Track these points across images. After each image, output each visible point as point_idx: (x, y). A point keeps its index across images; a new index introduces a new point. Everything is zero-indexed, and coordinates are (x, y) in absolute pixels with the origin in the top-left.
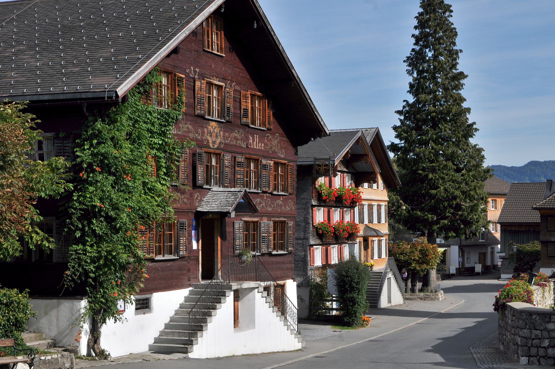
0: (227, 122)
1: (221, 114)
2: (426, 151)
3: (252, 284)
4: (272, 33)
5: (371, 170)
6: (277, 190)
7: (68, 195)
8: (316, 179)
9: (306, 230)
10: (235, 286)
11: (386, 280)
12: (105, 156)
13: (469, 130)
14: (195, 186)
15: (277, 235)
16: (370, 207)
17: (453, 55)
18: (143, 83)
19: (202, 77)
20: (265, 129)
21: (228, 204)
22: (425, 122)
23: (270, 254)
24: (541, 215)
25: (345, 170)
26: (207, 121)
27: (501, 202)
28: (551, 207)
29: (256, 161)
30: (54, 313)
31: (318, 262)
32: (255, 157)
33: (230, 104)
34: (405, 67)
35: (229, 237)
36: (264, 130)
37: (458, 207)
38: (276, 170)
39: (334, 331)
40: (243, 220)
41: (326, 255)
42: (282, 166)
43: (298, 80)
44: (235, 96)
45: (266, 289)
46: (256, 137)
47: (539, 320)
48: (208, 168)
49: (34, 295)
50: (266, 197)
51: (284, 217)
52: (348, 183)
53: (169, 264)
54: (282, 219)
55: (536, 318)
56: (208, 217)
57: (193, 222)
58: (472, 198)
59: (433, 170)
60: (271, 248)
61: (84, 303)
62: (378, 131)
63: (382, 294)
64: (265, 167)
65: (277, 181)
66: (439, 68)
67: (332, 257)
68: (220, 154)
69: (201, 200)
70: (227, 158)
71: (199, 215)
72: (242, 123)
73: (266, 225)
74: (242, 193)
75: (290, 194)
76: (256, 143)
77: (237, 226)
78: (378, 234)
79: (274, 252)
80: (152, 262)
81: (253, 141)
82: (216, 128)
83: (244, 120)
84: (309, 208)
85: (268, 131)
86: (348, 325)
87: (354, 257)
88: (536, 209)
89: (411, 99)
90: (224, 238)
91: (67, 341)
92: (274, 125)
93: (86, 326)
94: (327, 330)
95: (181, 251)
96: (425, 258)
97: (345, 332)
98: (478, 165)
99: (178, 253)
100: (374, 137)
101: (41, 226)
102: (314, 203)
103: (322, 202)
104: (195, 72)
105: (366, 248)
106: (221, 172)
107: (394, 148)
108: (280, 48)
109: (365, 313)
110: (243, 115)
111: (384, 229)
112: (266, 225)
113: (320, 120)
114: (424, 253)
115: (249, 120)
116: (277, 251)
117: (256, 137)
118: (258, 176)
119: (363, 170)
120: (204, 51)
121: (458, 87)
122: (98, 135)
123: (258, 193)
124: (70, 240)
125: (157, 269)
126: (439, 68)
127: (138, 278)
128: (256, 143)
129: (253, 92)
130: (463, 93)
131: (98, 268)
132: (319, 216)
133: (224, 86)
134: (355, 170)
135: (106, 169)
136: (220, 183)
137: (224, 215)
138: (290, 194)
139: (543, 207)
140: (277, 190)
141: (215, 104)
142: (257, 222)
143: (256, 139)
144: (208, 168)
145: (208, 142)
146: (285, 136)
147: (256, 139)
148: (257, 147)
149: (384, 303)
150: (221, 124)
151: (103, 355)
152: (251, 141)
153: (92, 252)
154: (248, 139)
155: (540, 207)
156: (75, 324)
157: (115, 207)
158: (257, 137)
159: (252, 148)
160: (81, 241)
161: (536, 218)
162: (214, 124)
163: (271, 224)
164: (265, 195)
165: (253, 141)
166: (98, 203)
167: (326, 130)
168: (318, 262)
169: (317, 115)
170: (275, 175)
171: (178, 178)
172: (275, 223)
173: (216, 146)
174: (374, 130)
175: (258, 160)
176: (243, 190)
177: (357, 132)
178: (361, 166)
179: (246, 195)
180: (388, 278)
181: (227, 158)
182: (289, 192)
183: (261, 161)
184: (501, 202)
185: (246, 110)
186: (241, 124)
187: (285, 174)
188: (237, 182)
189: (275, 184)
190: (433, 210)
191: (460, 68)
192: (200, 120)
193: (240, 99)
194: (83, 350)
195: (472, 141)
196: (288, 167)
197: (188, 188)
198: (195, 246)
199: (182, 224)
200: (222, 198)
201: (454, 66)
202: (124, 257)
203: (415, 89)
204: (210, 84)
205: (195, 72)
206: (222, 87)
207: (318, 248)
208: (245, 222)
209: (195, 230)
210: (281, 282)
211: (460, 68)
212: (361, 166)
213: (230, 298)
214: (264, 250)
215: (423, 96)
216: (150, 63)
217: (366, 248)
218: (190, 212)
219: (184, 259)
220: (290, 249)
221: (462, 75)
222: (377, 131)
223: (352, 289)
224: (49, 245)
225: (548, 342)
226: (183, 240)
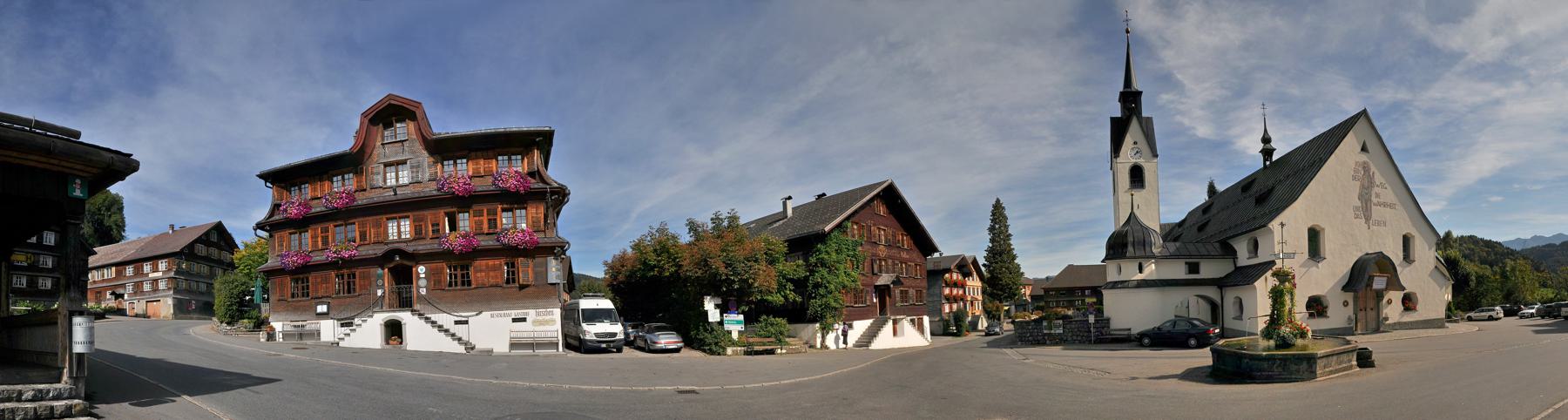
1: (886, 242)
2: (998, 266)
3: (902, 317)
7: (806, 278)
9: (941, 297)
10: (892, 317)
12: (822, 259)
13: (1014, 257)
14: (873, 274)
16: (973, 289)
17: (1007, 227)
18: (839, 226)
19: (874, 225)
22: (996, 254)
23: (914, 304)
27: (1031, 287)
29: (906, 263)
30: (806, 330)
31: (947, 310)
33: (890, 237)
34: (987, 232)
35: (893, 297)
37: (1011, 288)
41: (951, 308)
45: (912, 321)
48: (880, 266)
49: (790, 322)
52: (960, 277)
58: (1016, 284)
59: (1000, 274)
61: (818, 325)
66: (1001, 233)
67: (485, 189)
70: (890, 262)
73: (912, 292)
76: (904, 255)
78: (977, 300)
86: (959, 336)
87: (364, 152)
89: (991, 245)
90: (890, 297)
91: (812, 342)
92: (914, 247)
93: (819, 335)
94: (950, 338)
96: (998, 309)
97: (959, 338)
98: (1018, 271)
99: (866, 302)
101: (794, 290)
103: (947, 285)
105: (972, 305)
106: (887, 268)
107: (984, 265)
109: (414, 216)
111: (980, 298)
112: (912, 292)
114: (998, 308)
115: (900, 245)
118: (907, 270)
121: (1009, 239)
122: (818, 250)
124: (810, 297)
125: (855, 311)
126: (1001, 233)
127: (841, 314)
128: (904, 255)
130: (1011, 242)
131: (822, 309)
132: (947, 291)
135: (823, 265)
136: (887, 272)
137: (888, 286)
141: (883, 238)
144: (880, 266)
151: (827, 348)
153: (819, 302)
156: (815, 335)
157: (829, 282)
160: (815, 298)
161: (1042, 293)
166: (820, 280)
168: (947, 310)
171: (864, 269)
178: (965, 270)
181: (890, 262)
184: (1031, 287)
190: (1001, 290)
191: (1010, 232)
194: (819, 346)
195: (1016, 261)
197: (870, 275)
198: (875, 300)
199: (867, 292)
200: (886, 278)
201: (1007, 231)
202: (833, 304)
203: (992, 241)
204: (879, 228)
211: (1010, 232)
212: (965, 270)
213: (890, 324)
214: (911, 302)
215: (995, 244)
217: (972, 305)
221: (1010, 235)
223: (960, 321)
224: (799, 299)
226: (868, 298)
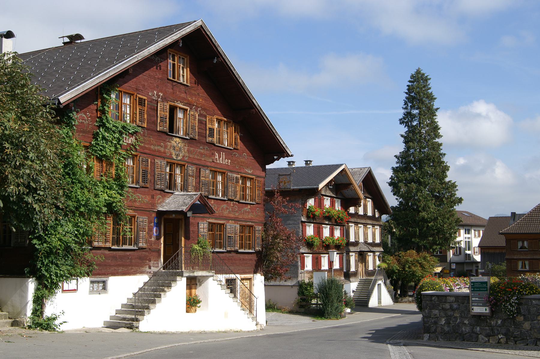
0: (191, 139)
4: (232, 68)
5: (357, 197)
6: (245, 199)
8: (306, 202)
11: (377, 286)
15: (245, 236)
19: (164, 99)
20: (231, 148)
21: (185, 204)
24: (506, 239)
25: (333, 195)
26: (171, 137)
28: (517, 232)
29: (223, 174)
32: (221, 170)
36: (231, 149)
38: (244, 183)
39: (313, 321)
40: (208, 222)
42: (251, 180)
43: (259, 109)
44: (201, 118)
46: (223, 154)
47: (437, 301)
50: (233, 204)
51: (252, 222)
53: (128, 253)
54: (250, 224)
55: (435, 299)
56: (171, 217)
57: (155, 219)
60: (237, 246)
62: (371, 169)
63: (372, 296)
64: (232, 179)
65: (245, 192)
68: (184, 165)
69: (163, 202)
70: (191, 169)
71: (160, 214)
72: (207, 141)
74: (197, 196)
75: (257, 204)
77: (201, 226)
79: (241, 251)
80: (109, 251)
81: (219, 157)
82: (180, 144)
83: (209, 139)
84: (299, 223)
85: (235, 150)
88: (502, 234)
95: (140, 243)
99: (136, 243)
100: (367, 174)
102: (303, 220)
103: (312, 217)
104: (158, 96)
108: (240, 81)
110: (208, 135)
113: (282, 143)
116: (245, 250)
117: (223, 154)
119: (350, 197)
120: (168, 79)
123: (225, 200)
129: (220, 118)
133: (189, 110)
134: (344, 197)
138: (257, 204)
139: (507, 232)
140: (245, 199)
142: (223, 224)
143: (223, 156)
145: (171, 154)
146: (251, 156)
147: (223, 156)
148: (223, 162)
149: (373, 302)
150: (184, 140)
152: (217, 157)
154: (213, 154)
155: (505, 232)
158: (223, 155)
159: (218, 163)
162: (178, 139)
163: (238, 226)
164: (232, 203)
165: (219, 157)
167: (288, 152)
169: (279, 138)
170: (243, 187)
172: (242, 226)
173: (179, 158)
174: (367, 169)
175: (224, 173)
176: (199, 193)
177: (341, 165)
179: (201, 197)
180: (378, 285)
182: (256, 202)
183: (227, 174)
185: (212, 130)
186: (207, 142)
187: (253, 187)
188: (202, 190)
189: (243, 194)
192: (164, 136)
193: (206, 122)
196: (255, 181)
200: (181, 200)
205: (158, 96)
206: (187, 110)
207: (308, 256)
208: (209, 223)
209: (156, 226)
210: (379, 305)
213: (181, 284)
216: (97, 78)
218: (151, 211)
219: (144, 250)
220: (257, 248)
222: (369, 170)
225: (444, 320)
